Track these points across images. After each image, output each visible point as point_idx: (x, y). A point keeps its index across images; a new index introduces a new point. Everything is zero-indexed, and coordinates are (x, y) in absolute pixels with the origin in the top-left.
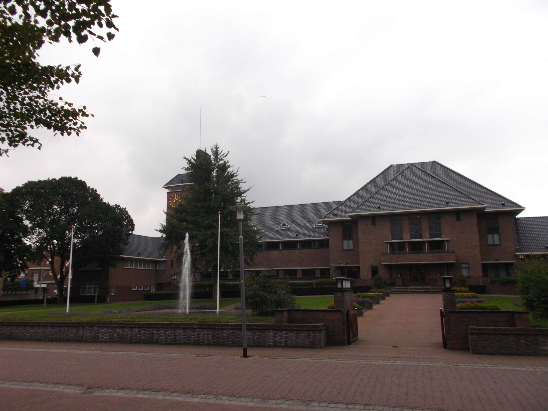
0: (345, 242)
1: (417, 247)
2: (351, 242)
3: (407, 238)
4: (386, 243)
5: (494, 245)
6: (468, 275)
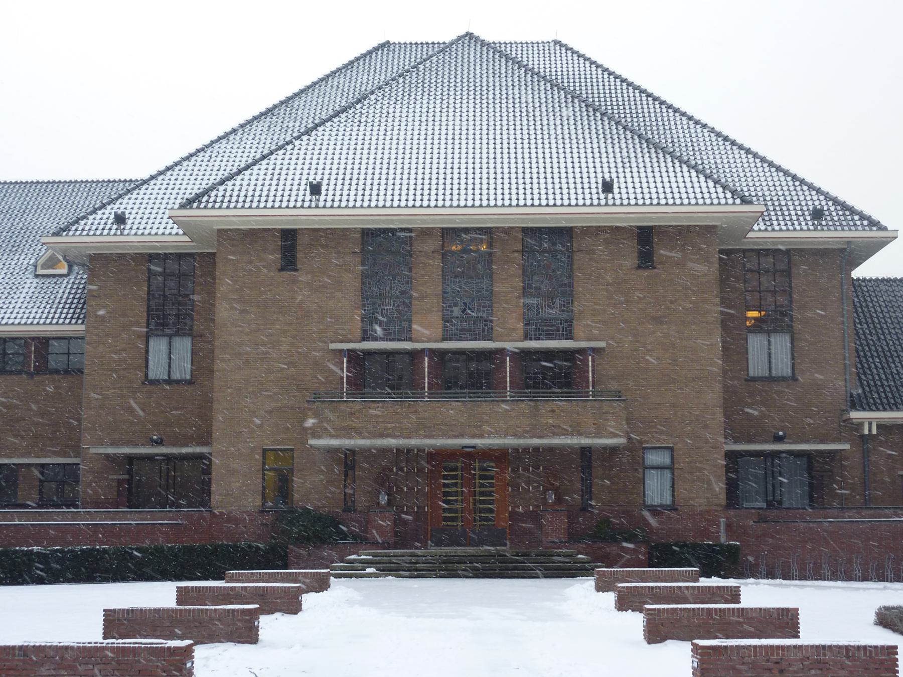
0: (158, 347)
1: (468, 375)
2: (183, 346)
3: (426, 335)
5: (771, 379)
6: (668, 500)
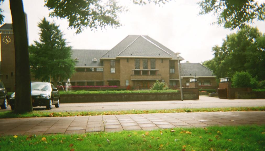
1: (145, 73)
4: (133, 70)
5: (173, 73)
